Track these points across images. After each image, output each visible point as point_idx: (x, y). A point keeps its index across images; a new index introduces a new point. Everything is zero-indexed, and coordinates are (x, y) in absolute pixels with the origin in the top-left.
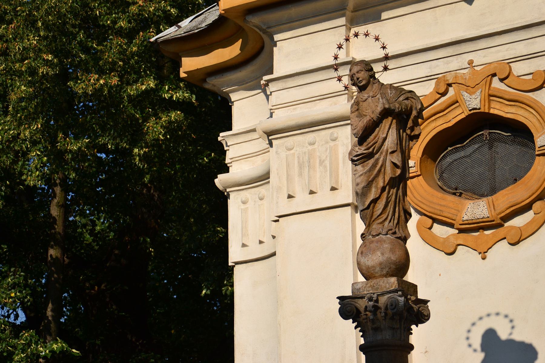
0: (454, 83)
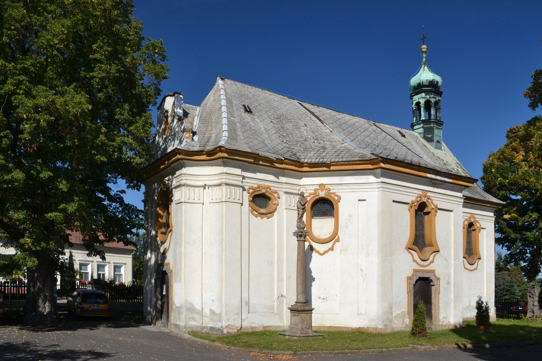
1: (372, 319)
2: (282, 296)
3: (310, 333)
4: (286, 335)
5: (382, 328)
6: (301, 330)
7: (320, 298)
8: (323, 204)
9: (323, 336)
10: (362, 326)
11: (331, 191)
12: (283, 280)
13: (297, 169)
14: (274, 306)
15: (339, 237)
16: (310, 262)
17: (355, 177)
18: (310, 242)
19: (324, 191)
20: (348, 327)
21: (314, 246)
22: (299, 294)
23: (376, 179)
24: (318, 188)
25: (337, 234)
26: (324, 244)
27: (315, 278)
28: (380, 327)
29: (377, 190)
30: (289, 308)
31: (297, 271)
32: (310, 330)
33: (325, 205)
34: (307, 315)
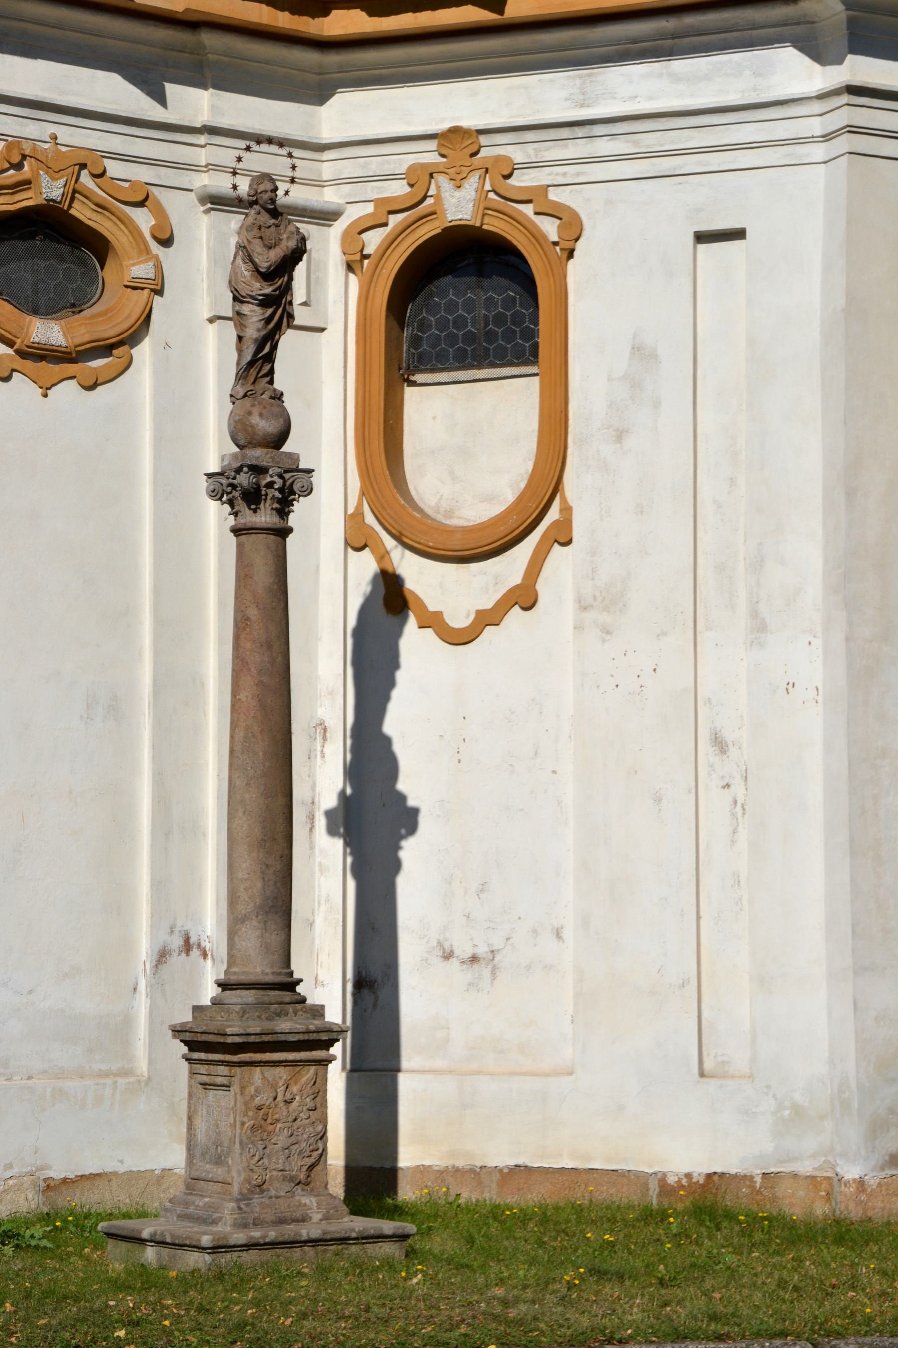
0: (31, 157)
1: (798, 1111)
2: (187, 946)
3: (316, 1217)
4: (142, 1241)
5: (872, 1182)
6: (244, 1197)
7: (448, 956)
8: (473, 279)
9: (403, 1237)
10: (733, 1168)
11: (521, 180)
12: (194, 830)
13: (284, 20)
14: (127, 1022)
15: (567, 510)
16: (386, 699)
17: (680, 66)
18: (382, 556)
19: (473, 181)
20: (638, 1175)
21: (412, 583)
22: (243, 921)
23: (816, 66)
24: (434, 158)
25: (557, 487)
26: (474, 566)
27: (415, 812)
28: (851, 1172)
29: (819, 151)
30: (178, 1032)
31: (232, 751)
32: (312, 1192)
33: (486, 282)
34: (294, 1078)
